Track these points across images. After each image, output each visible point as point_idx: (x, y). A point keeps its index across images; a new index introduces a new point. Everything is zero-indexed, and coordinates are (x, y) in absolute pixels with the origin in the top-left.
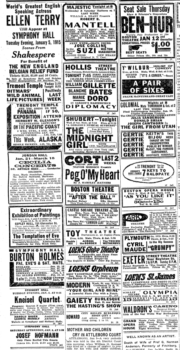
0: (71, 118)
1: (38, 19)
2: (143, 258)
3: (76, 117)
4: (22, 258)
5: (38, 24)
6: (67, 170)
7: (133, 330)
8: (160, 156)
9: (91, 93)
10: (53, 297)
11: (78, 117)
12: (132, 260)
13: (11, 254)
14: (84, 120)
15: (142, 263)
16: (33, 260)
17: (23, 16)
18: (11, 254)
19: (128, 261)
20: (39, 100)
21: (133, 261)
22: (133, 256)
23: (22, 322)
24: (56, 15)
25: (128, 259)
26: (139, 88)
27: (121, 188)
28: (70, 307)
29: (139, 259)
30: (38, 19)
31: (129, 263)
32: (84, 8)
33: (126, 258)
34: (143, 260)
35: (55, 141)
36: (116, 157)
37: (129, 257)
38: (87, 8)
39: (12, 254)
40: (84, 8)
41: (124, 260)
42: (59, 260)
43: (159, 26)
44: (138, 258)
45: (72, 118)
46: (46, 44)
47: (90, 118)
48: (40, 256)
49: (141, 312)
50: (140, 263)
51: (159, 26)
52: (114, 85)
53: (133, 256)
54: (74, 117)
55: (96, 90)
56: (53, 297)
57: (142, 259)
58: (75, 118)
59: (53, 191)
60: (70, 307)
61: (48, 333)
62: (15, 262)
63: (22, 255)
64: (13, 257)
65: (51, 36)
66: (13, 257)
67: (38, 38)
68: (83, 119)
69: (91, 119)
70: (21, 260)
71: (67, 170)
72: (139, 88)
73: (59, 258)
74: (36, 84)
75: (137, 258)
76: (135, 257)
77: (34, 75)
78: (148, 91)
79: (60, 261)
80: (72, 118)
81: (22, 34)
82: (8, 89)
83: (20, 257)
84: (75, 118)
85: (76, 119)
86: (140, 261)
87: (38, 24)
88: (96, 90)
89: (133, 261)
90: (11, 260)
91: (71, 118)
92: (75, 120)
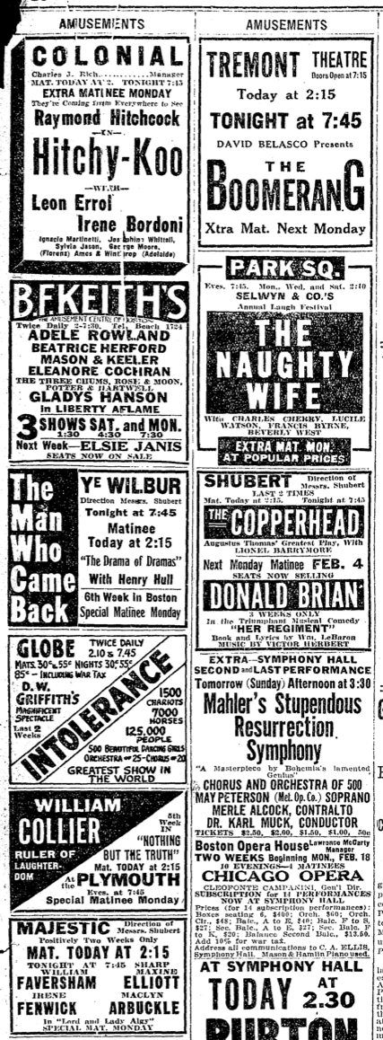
0: (219, 477)
1: (215, 990)
2: (225, 61)
3: (236, 476)
5: (215, 1007)
6: (211, 163)
8: (163, 923)
9: (149, 489)
10: (159, 218)
11: (243, 476)
14: (260, 485)
23: (136, 513)
24: (228, 75)
27: (373, 248)
28: (170, 884)
30: (215, 990)
32: (84, 932)
35: (171, 492)
36: (310, 997)
38: (93, 932)
40: (84, 932)
44: (286, 187)
45: (223, 477)
46: (53, 124)
47: (278, 478)
54: (229, 476)
56: (159, 218)
58: (233, 477)
60: (170, 884)
61: (157, 420)
67: (283, 126)
68: (256, 481)
69: (282, 482)
71: (211, 163)
80: (223, 477)
82: (216, 1015)
84: (233, 477)
85: (237, 482)
87: (215, 1007)
91: (219, 477)
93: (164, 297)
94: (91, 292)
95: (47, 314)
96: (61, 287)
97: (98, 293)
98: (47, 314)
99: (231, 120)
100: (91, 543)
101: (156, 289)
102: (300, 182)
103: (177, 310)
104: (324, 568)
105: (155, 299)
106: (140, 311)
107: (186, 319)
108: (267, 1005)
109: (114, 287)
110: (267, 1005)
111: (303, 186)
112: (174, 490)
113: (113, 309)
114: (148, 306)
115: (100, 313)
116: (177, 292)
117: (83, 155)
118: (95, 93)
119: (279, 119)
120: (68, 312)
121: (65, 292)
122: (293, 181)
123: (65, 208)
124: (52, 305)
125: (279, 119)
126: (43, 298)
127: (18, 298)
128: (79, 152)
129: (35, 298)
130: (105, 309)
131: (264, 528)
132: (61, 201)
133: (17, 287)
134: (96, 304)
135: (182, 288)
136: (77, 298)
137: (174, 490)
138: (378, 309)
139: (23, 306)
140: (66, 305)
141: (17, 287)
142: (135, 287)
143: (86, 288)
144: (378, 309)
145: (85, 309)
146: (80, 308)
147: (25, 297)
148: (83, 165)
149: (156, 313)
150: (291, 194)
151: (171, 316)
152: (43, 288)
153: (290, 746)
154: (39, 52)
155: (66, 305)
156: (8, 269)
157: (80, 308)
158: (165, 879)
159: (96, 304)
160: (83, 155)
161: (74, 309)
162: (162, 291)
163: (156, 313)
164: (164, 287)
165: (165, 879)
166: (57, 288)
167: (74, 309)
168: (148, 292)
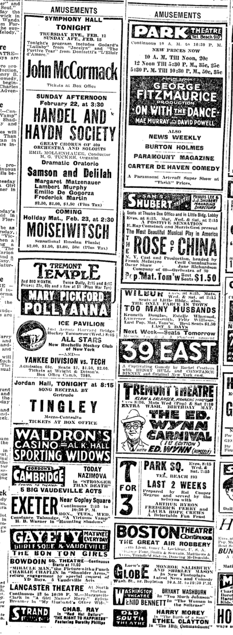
2: (54, 503)
7: (40, 93)
12: (30, 505)
15: (52, 513)
19: (23, 507)
22: (33, 498)
25: (23, 503)
26: (215, 93)
29: (45, 505)
31: (25, 513)
33: (17, 502)
41: (14, 505)
43: (62, 114)
44: (44, 502)
48: (108, 233)
49: (44, 223)
50: (48, 513)
51: (62, 114)
53: (33, 498)
59: (160, 402)
72: (215, 93)
75: (42, 501)
76: (38, 498)
77: (69, 204)
78: (38, 446)
86: (48, 509)
87: (70, 402)
92: (52, 126)
99: (133, 573)
100: (159, 276)
102: (52, 498)
108: (36, 137)
110: (36, 137)
111: (54, 501)
117: (90, 130)
118: (71, 588)
119: (87, 28)
122: (48, 498)
123: (56, 176)
125: (87, 28)
128: (89, 129)
131: (23, 457)
132: (54, 171)
148: (100, 235)
150: (47, 505)
153: (40, 66)
160: (90, 130)
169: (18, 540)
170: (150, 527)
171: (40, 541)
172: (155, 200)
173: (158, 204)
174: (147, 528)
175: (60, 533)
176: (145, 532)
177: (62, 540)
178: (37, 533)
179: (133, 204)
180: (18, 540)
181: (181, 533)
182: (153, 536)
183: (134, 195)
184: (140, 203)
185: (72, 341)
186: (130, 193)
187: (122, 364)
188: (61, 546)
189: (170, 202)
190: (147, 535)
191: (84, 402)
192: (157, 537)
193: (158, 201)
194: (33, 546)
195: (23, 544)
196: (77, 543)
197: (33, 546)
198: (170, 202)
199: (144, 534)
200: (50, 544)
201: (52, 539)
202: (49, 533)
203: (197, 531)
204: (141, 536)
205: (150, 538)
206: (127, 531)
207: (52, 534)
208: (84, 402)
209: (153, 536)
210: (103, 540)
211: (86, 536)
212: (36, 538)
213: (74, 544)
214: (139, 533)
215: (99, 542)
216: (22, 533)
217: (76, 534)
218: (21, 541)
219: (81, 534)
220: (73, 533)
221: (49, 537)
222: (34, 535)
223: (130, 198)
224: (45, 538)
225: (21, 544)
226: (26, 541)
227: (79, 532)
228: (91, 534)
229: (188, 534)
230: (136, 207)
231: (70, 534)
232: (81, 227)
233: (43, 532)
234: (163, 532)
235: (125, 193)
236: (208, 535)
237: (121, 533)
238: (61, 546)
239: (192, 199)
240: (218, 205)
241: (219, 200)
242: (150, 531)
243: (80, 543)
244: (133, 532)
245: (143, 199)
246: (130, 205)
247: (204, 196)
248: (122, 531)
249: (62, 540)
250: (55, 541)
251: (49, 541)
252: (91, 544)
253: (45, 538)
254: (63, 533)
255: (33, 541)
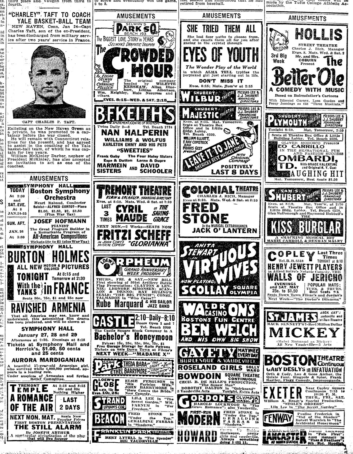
4: (26, 258)
13: (9, 252)
16: (43, 261)
17: (57, 283)
18: (9, 252)
19: (272, 394)
20: (86, 267)
21: (282, 395)
29: (292, 393)
33: (268, 391)
34: (299, 393)
37: (274, 388)
39: (11, 252)
42: (82, 261)
44: (185, 51)
52: (206, 207)
55: (247, 171)
57: (298, 393)
62: (16, 265)
63: (27, 254)
64: (13, 256)
65: (252, 30)
66: (13, 256)
70: (24, 262)
73: (82, 259)
74: (161, 334)
76: (285, 388)
79: (84, 263)
81: (148, 188)
83: (23, 257)
87: (24, 410)
88: (247, 171)
89: (282, 395)
90: (9, 262)
93: (164, 112)
94: (131, 110)
95: (111, 121)
96: (118, 108)
97: (135, 111)
98: (111, 121)
101: (161, 109)
103: (170, 118)
104: (150, 135)
105: (160, 113)
106: (153, 119)
107: (174, 123)
109: (142, 108)
112: (299, 31)
113: (142, 119)
114: (157, 117)
115: (135, 120)
116: (170, 110)
120: (120, 119)
121: (119, 110)
124: (114, 116)
126: (109, 113)
127: (98, 113)
129: (105, 113)
130: (138, 119)
133: (97, 108)
134: (133, 116)
135: (173, 108)
136: (125, 113)
137: (299, 31)
138: (111, 5)
139: (100, 117)
140: (120, 116)
141: (97, 108)
142: (151, 108)
143: (129, 108)
144: (111, 5)
145: (129, 118)
146: (126, 117)
147: (101, 113)
149: (161, 120)
151: (167, 121)
152: (109, 108)
154: (272, 255)
155: (120, 116)
156: (15, 108)
157: (126, 117)
158: (18, 427)
159: (133, 116)
161: (123, 118)
162: (163, 109)
163: (161, 120)
164: (164, 108)
165: (18, 427)
166: (116, 108)
167: (123, 118)
168: (157, 110)
169: (183, 355)
170: (292, 356)
171: (202, 356)
172: (292, 194)
173: (294, 197)
174: (289, 356)
175: (218, 350)
176: (287, 360)
177: (221, 356)
178: (199, 349)
179: (273, 198)
180: (183, 355)
181: (318, 361)
182: (295, 364)
183: (274, 190)
184: (279, 197)
185: (49, 429)
186: (270, 189)
187: (267, 203)
188: (219, 360)
189: (304, 195)
190: (290, 363)
191: (227, 215)
192: (298, 365)
193: (294, 195)
194: (196, 360)
195: (188, 358)
196: (232, 358)
197: (196, 360)
198: (304, 195)
199: (287, 362)
200: (211, 358)
201: (212, 355)
202: (210, 349)
203: (331, 359)
204: (284, 364)
205: (292, 365)
206: (273, 360)
207: (212, 350)
208: (227, 215)
209: (295, 364)
210: (254, 356)
211: (240, 352)
212: (199, 354)
213: (230, 359)
214: (283, 361)
215: (250, 357)
216: (187, 349)
217: (232, 350)
218: (186, 356)
219: (236, 351)
220: (229, 350)
221: (210, 353)
222: (197, 351)
223: (270, 192)
224: (206, 353)
225: (186, 358)
226: (190, 357)
227: (234, 349)
228: (243, 350)
229: (323, 361)
230: (275, 200)
231: (227, 350)
232: (246, 51)
233: (204, 349)
234: (303, 360)
235: (266, 189)
236: (341, 362)
237: (269, 362)
238: (219, 360)
239: (322, 192)
240: (343, 197)
241: (344, 193)
242: (292, 359)
243: (234, 358)
244: (277, 360)
245: (282, 193)
246: (270, 199)
247: (331, 190)
248: (269, 360)
249: (221, 356)
250: (214, 356)
251: (209, 356)
252: (244, 359)
253: (206, 353)
254: (221, 350)
255: (196, 356)
